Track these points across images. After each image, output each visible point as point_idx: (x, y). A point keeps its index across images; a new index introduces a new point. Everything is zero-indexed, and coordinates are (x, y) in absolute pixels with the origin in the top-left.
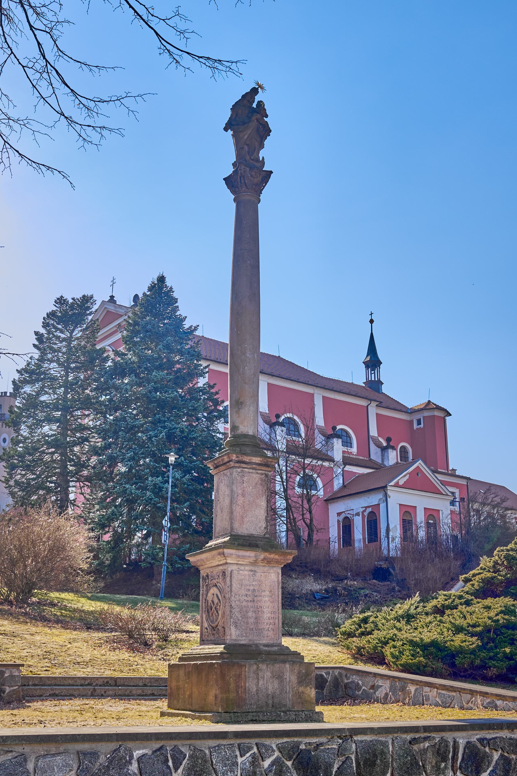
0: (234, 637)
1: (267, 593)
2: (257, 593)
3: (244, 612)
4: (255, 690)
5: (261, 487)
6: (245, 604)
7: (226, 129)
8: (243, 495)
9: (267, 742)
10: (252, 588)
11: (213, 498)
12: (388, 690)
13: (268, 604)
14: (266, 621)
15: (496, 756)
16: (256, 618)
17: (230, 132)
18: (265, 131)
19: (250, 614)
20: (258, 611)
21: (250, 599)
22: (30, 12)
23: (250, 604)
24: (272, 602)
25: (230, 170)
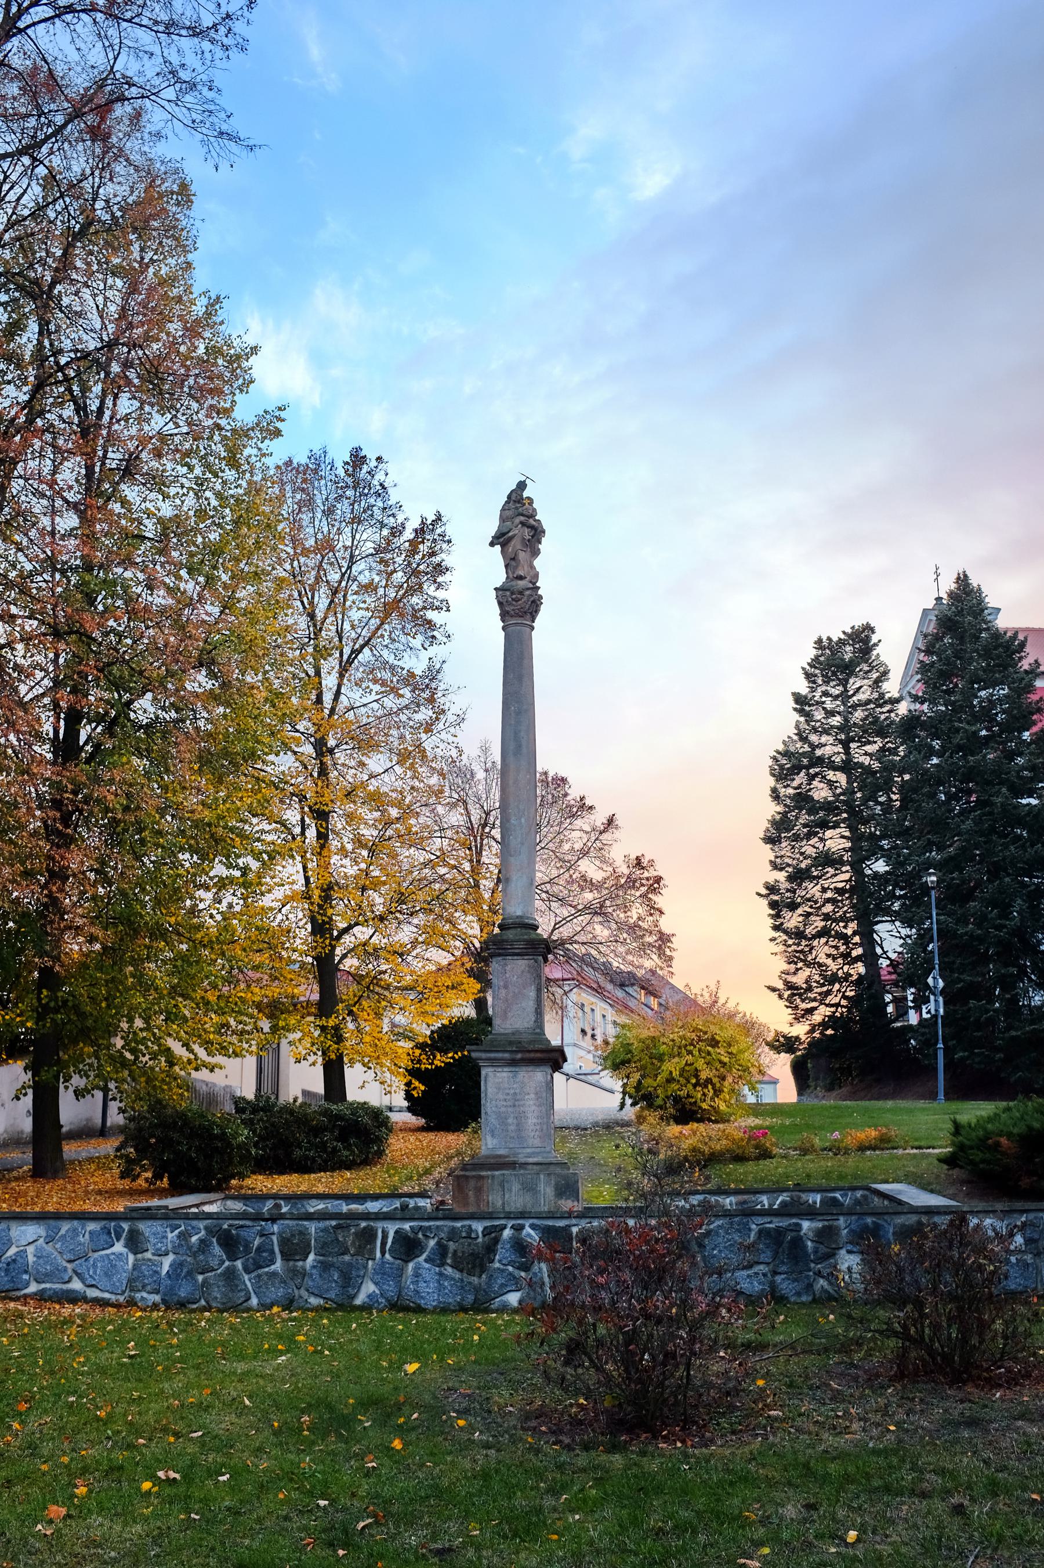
0: (490, 1146)
1: (532, 1096)
2: (518, 1097)
3: (503, 1119)
4: (500, 1202)
5: (528, 975)
6: (503, 1109)
7: (492, 544)
8: (506, 987)
9: (194, 1223)
10: (512, 1091)
11: (490, 1012)
12: (270, 1092)
13: (533, 1108)
14: (531, 1128)
15: (432, 1243)
16: (518, 1125)
17: (498, 548)
18: (537, 532)
19: (510, 1121)
20: (520, 1118)
21: (509, 1103)
22: (340, 622)
23: (510, 1109)
24: (540, 1106)
25: (533, 633)
